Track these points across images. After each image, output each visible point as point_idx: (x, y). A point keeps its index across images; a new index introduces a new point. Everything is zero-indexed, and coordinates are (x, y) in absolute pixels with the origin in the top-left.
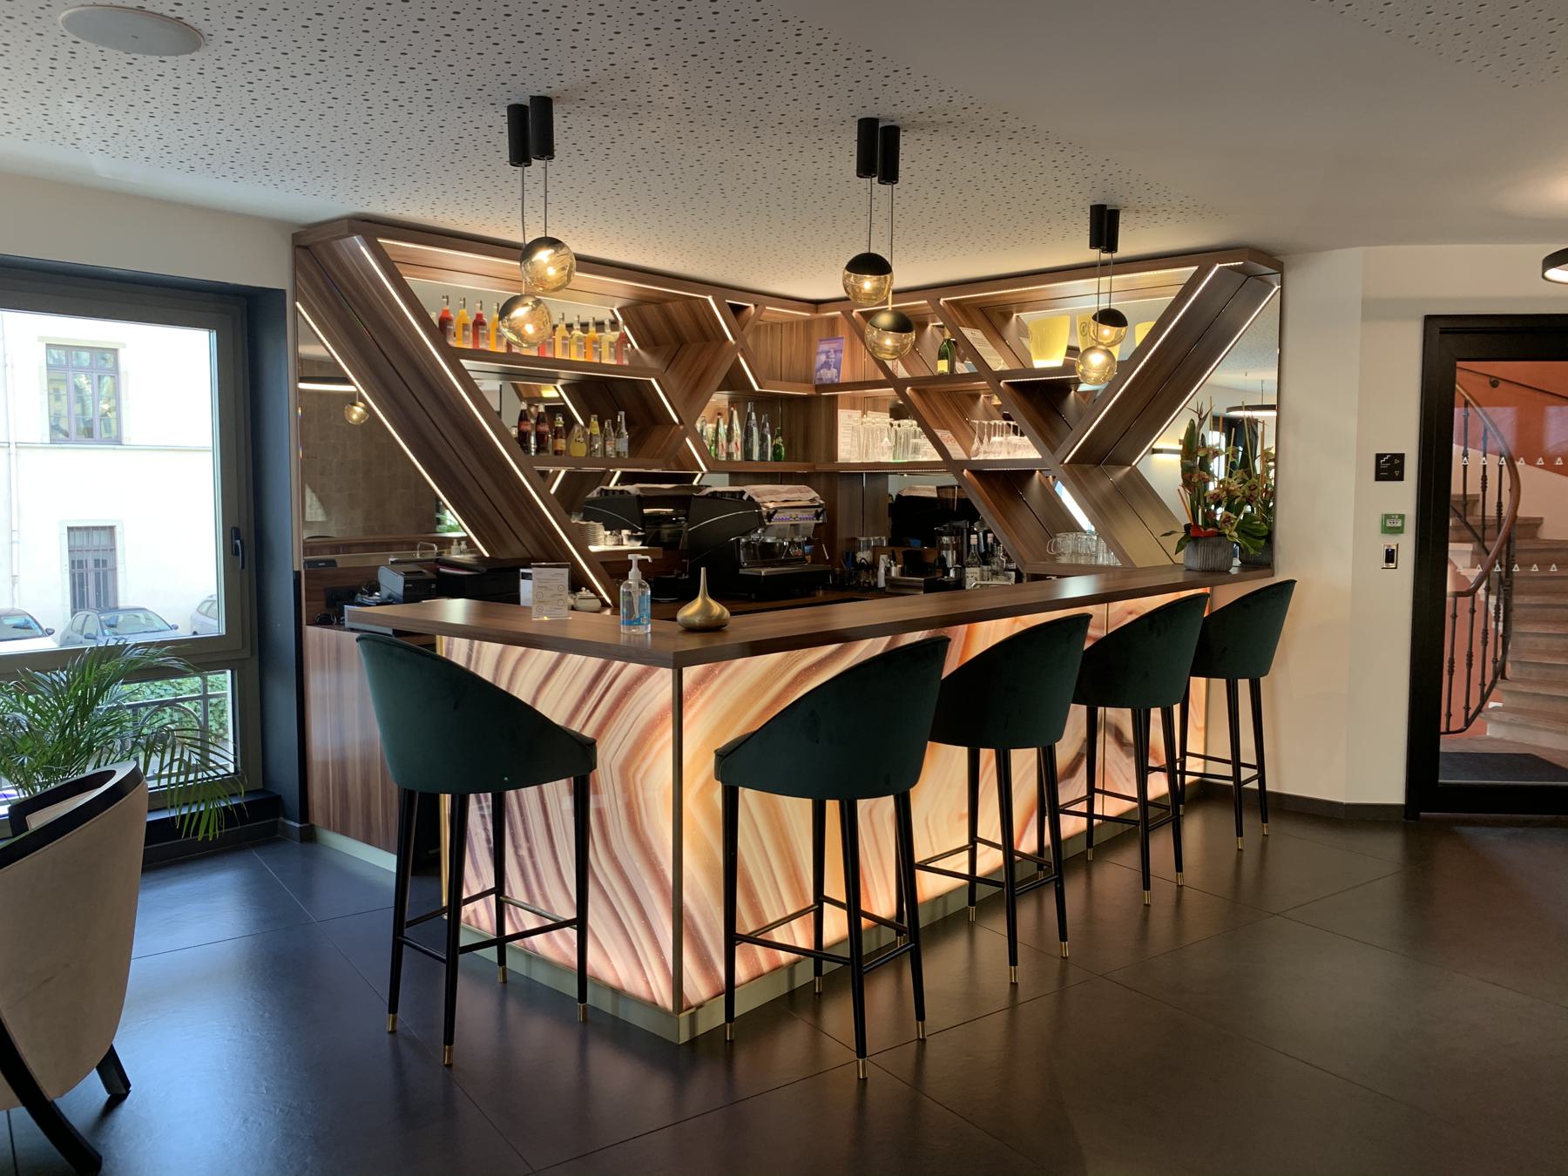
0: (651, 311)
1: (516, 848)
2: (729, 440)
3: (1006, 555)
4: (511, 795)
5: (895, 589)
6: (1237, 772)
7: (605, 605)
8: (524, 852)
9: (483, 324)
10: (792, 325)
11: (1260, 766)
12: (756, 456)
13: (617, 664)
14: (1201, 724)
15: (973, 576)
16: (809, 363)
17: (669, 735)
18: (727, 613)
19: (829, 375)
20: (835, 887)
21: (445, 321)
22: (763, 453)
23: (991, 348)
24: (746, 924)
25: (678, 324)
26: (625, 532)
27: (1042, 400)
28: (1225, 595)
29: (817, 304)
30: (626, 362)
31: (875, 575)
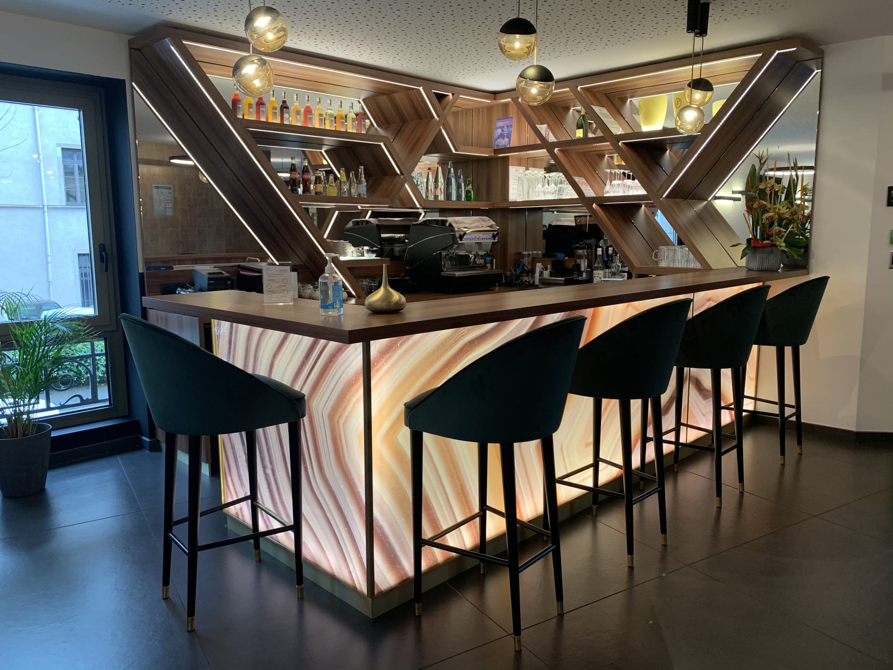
0: (384, 100)
1: (264, 467)
2: (436, 187)
3: (621, 262)
4: (260, 431)
5: (546, 284)
6: (782, 410)
7: (350, 295)
8: (269, 471)
9: (263, 104)
10: (479, 110)
11: (798, 406)
12: (454, 198)
13: (322, 342)
14: (754, 376)
15: (599, 275)
16: (490, 135)
17: (361, 392)
18: (403, 299)
19: (503, 142)
20: (496, 499)
21: (236, 102)
22: (459, 196)
23: (613, 120)
24: (427, 533)
25: (404, 108)
26: (366, 248)
27: (646, 153)
28: (777, 288)
29: (495, 94)
30: (364, 132)
31: (533, 277)
